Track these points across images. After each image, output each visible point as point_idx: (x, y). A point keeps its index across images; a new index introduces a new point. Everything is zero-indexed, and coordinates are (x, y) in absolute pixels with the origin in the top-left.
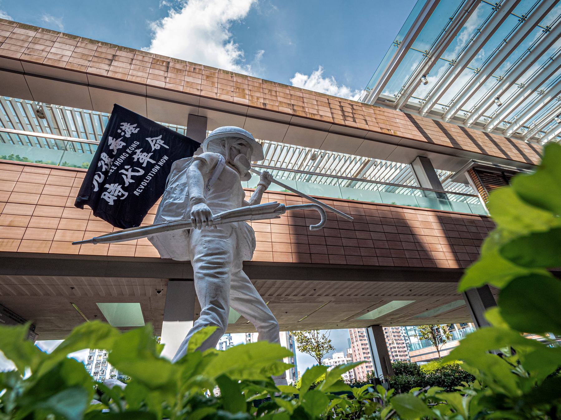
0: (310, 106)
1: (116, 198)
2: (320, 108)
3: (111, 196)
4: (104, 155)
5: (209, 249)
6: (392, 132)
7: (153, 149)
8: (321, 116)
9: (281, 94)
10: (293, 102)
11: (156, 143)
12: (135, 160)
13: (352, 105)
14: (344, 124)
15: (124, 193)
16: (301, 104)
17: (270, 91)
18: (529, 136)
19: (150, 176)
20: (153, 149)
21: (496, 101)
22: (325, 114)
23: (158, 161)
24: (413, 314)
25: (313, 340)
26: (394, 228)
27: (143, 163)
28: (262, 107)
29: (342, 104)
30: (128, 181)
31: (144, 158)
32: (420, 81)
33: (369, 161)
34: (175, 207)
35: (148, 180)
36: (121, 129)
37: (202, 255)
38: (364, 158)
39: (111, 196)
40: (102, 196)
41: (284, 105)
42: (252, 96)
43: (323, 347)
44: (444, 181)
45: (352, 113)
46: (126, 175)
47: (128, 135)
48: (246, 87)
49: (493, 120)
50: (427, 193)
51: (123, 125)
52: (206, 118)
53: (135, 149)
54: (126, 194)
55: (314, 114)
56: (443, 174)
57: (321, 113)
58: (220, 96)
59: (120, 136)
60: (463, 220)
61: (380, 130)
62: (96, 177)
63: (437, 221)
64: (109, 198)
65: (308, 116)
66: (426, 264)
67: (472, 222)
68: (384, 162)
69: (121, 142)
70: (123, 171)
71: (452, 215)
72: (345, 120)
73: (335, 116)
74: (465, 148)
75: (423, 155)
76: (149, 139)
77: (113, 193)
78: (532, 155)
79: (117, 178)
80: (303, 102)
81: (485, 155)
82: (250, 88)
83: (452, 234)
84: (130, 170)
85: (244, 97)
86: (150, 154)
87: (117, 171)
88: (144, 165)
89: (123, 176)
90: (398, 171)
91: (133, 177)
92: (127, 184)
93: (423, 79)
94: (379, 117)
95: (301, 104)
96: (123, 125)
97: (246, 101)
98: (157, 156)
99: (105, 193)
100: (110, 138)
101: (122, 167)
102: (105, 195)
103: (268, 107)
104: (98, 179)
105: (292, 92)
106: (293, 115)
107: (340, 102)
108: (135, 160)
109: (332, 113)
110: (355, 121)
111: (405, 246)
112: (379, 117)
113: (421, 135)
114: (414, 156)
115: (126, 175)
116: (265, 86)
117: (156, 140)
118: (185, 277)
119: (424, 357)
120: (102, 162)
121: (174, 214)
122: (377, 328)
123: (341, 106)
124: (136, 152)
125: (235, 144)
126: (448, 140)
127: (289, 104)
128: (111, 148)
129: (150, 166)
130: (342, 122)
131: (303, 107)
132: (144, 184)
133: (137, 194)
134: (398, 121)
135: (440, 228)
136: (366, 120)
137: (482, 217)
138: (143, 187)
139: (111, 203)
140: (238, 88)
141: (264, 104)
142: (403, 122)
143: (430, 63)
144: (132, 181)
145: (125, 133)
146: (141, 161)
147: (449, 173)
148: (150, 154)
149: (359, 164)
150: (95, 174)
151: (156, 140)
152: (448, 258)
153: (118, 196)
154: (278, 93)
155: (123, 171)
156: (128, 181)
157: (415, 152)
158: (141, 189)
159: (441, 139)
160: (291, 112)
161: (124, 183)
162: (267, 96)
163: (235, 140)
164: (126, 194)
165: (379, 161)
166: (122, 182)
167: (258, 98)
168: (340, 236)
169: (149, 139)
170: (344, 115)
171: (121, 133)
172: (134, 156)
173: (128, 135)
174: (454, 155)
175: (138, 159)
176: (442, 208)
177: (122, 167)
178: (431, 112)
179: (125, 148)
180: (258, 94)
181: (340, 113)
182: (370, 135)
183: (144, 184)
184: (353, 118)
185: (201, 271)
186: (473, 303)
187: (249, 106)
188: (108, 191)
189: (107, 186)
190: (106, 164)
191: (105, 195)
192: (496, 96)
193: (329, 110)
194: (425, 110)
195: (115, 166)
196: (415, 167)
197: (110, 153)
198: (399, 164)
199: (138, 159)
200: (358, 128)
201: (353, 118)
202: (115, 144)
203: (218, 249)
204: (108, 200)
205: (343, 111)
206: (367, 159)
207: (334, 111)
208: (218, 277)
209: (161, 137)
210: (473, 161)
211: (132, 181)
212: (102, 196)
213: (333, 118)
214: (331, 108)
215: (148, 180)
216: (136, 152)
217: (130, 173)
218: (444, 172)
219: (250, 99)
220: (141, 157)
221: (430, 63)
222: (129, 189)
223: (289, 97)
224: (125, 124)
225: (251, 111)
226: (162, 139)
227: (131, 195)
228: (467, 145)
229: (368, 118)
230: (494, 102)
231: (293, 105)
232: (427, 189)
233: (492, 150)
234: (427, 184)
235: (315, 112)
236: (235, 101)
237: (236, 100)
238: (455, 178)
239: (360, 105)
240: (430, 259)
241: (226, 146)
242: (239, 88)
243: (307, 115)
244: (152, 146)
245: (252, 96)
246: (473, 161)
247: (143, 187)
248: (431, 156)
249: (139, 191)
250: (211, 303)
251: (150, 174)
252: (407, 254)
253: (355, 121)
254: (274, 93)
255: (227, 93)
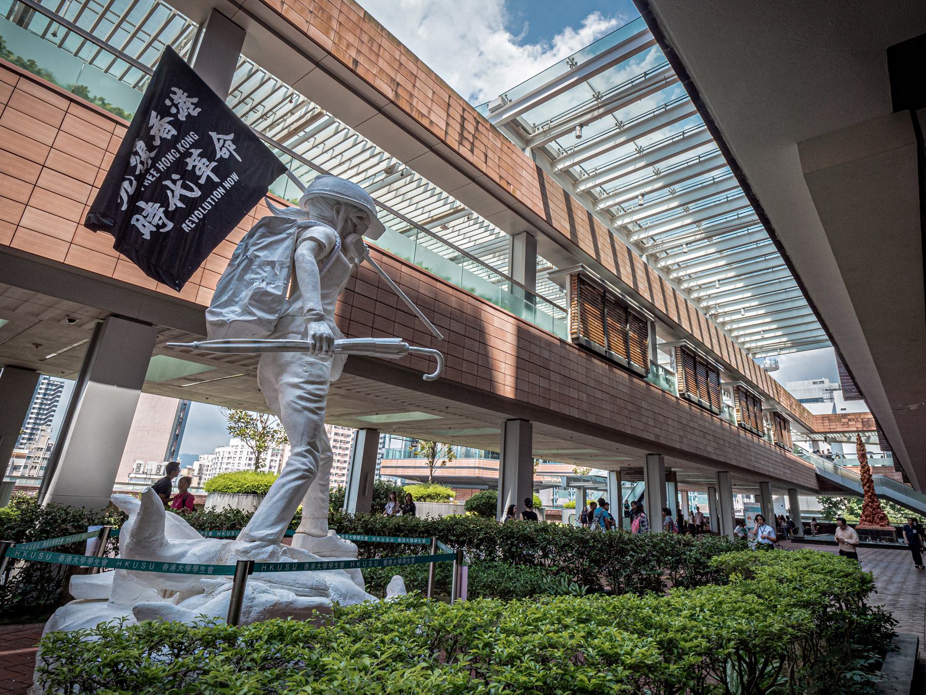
0: (421, 97)
1: (155, 229)
2: (435, 108)
3: (146, 224)
4: (140, 145)
5: (311, 375)
6: (511, 189)
7: (218, 156)
8: (431, 122)
9: (386, 54)
10: (399, 78)
11: (223, 146)
12: (189, 168)
13: (478, 122)
14: (456, 148)
15: (166, 221)
16: (409, 87)
17: (372, 40)
18: (651, 251)
19: (209, 202)
20: (218, 156)
21: (640, 197)
22: (438, 120)
23: (223, 178)
24: (428, 429)
25: (259, 423)
26: (462, 326)
27: (199, 177)
28: (351, 66)
29: (466, 115)
30: (175, 203)
31: (204, 169)
32: (574, 129)
33: (463, 209)
34: (270, 298)
35: (205, 209)
36: (172, 100)
37: (302, 380)
38: (458, 203)
39: (146, 224)
40: (133, 222)
41: (384, 77)
42: (340, 37)
43: (273, 436)
44: (540, 271)
45: (474, 136)
46: (173, 191)
47: (182, 117)
48: (335, 13)
49: (627, 214)
50: (516, 287)
51: (175, 93)
52: (243, 30)
53: (192, 147)
54: (170, 225)
55: (423, 115)
56: (543, 262)
57: (433, 117)
58: (287, 10)
59: (170, 115)
60: (540, 339)
61: (497, 180)
62: (126, 184)
63: (515, 333)
64: (144, 226)
65: (413, 114)
66: (482, 385)
67: (549, 344)
68: (481, 219)
69: (170, 127)
70: (168, 183)
71: (532, 329)
72: (460, 143)
73: (450, 131)
74: (582, 245)
75: (531, 232)
76: (213, 135)
77: (150, 219)
78: (642, 280)
79: (159, 195)
80: (414, 86)
81: (597, 264)
82: (342, 19)
83: (526, 356)
84: (179, 183)
85: (327, 34)
86: (214, 164)
87: (159, 180)
88: (202, 181)
89: (169, 192)
90: (493, 237)
91: (183, 198)
92: (172, 208)
93: (578, 128)
94: (504, 157)
95: (409, 87)
96: (175, 93)
97: (328, 43)
98: (223, 168)
99: (137, 216)
100: (154, 114)
101: (166, 175)
102: (138, 220)
103: (360, 71)
104: (127, 188)
105: (404, 60)
106: (392, 102)
107: (464, 110)
108: (189, 168)
109: (447, 124)
110: (472, 151)
111: (467, 355)
112: (504, 157)
113: (542, 207)
114: (521, 229)
115: (173, 191)
116: (366, 26)
117: (225, 141)
118: (141, 318)
119: (400, 472)
120: (138, 157)
121: (266, 308)
122: (373, 433)
123: (462, 117)
124: (191, 154)
125: (353, 216)
126: (568, 227)
127: (393, 80)
128: (152, 133)
129: (209, 187)
130: (455, 146)
131: (411, 95)
132: (198, 214)
133: (186, 229)
134: (524, 173)
135: (515, 343)
136: (486, 156)
137: (561, 340)
138: (197, 221)
139: (147, 236)
140: (321, 8)
141: (356, 62)
142: (529, 178)
143: (596, 113)
144: (180, 205)
145: (178, 112)
146: (198, 173)
147: (549, 264)
148: (214, 164)
149: (448, 207)
150: (124, 179)
151: (225, 141)
152: (508, 383)
153: (158, 226)
154: (382, 50)
155: (168, 183)
156: (175, 203)
157: (523, 225)
158: (193, 222)
159: (561, 224)
160: (391, 95)
161: (168, 206)
162: (364, 50)
163: (355, 210)
164: (170, 225)
165: (475, 215)
166: (165, 203)
167: (349, 45)
168: (393, 319)
169: (213, 135)
170: (461, 135)
171: (170, 107)
172: (188, 160)
173: (182, 117)
174: (566, 247)
175: (194, 167)
176: (525, 316)
177: (166, 175)
178: (566, 172)
179: (176, 140)
180: (350, 38)
181: (458, 128)
182: (483, 179)
183: (198, 214)
184: (472, 144)
185: (300, 402)
186: (508, 437)
187: (329, 53)
188: (144, 213)
189: (141, 204)
190: (142, 163)
191: (138, 220)
192: (643, 191)
193: (444, 116)
194: (560, 166)
195: (158, 170)
196: (516, 241)
197: (149, 141)
198: (497, 230)
199: (194, 167)
200: (472, 164)
201: (472, 144)
202: (162, 129)
203: (320, 377)
204: (142, 230)
205: (462, 126)
206: (463, 206)
207: (451, 122)
208: (317, 414)
209: (231, 136)
210: (582, 267)
211: (180, 205)
212: (133, 222)
213: (446, 133)
214: (448, 115)
215: (205, 209)
216: (191, 154)
217: (179, 190)
218: (545, 261)
219: (336, 41)
220: (199, 165)
221: (596, 113)
222: (175, 216)
223: (396, 66)
224: (179, 92)
225: (329, 62)
226: (233, 141)
227: (178, 229)
228: (586, 244)
229: (490, 154)
230: (637, 197)
231: (398, 84)
232: (518, 284)
233: (607, 260)
234: (520, 277)
235: (425, 112)
236: (310, 34)
237: (313, 32)
238: (553, 276)
239: (488, 127)
240: (491, 381)
241: (341, 213)
242: (324, 11)
243: (412, 111)
244: (218, 149)
245: (340, 37)
246: (582, 267)
247: (197, 221)
248: (540, 237)
249: (190, 224)
250: (309, 444)
251: (209, 200)
252: (465, 367)
253: (472, 151)
254: (375, 48)
255: (301, 12)
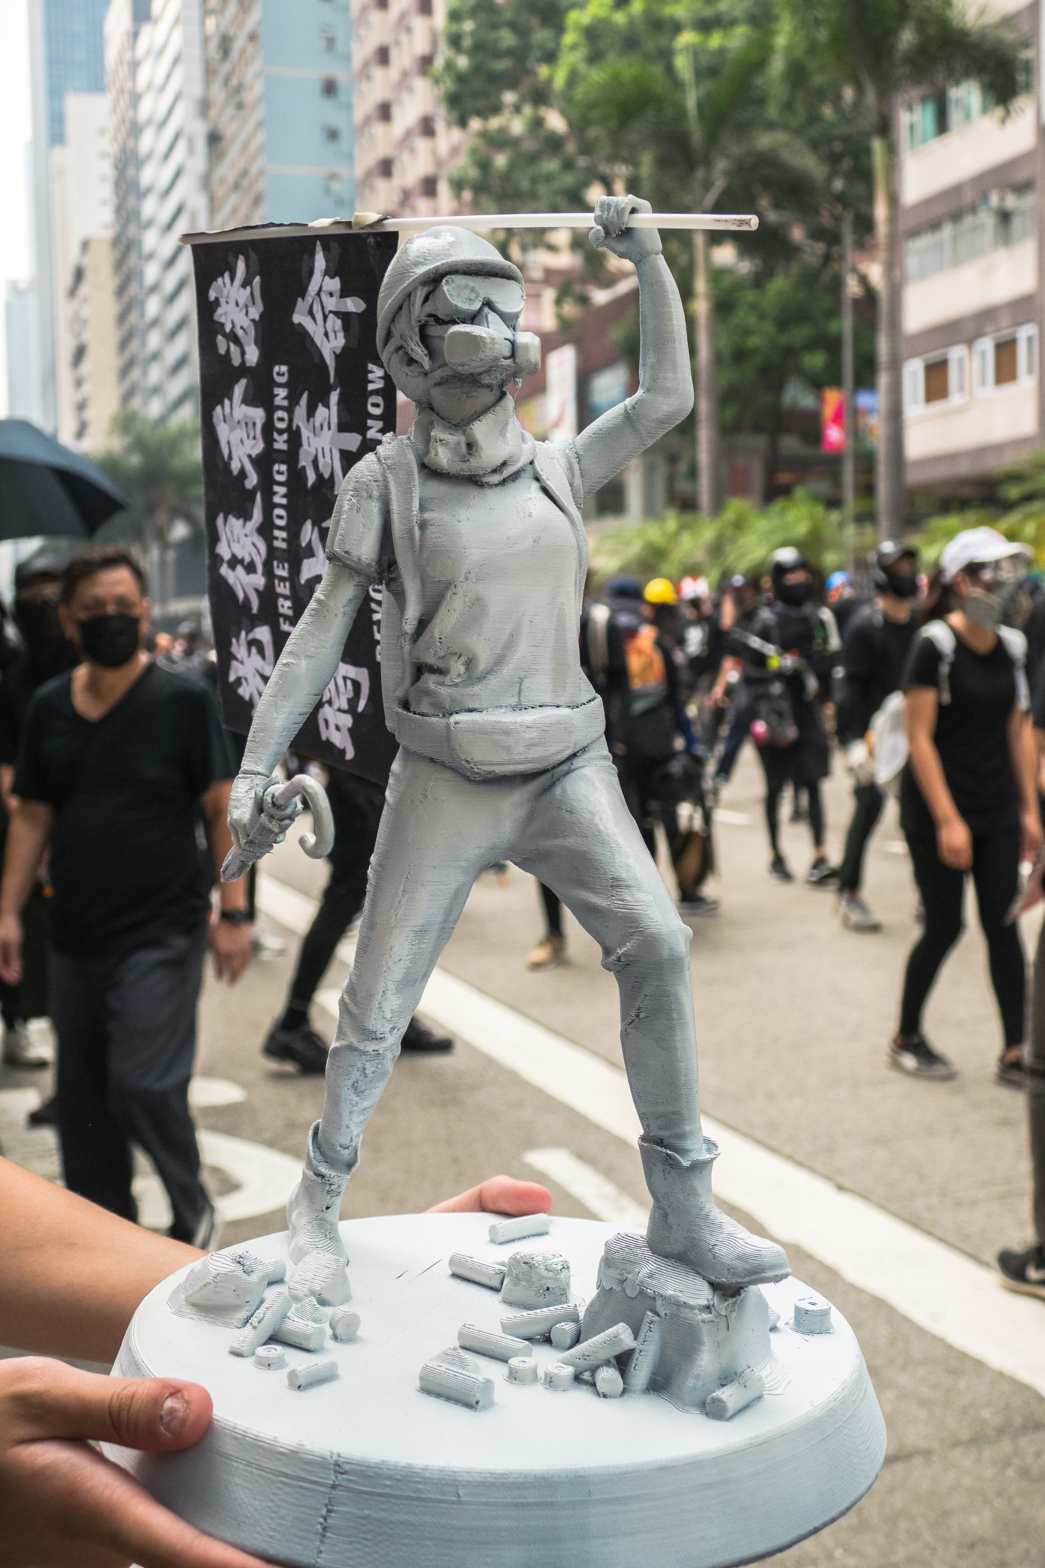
11: (325, 318)
